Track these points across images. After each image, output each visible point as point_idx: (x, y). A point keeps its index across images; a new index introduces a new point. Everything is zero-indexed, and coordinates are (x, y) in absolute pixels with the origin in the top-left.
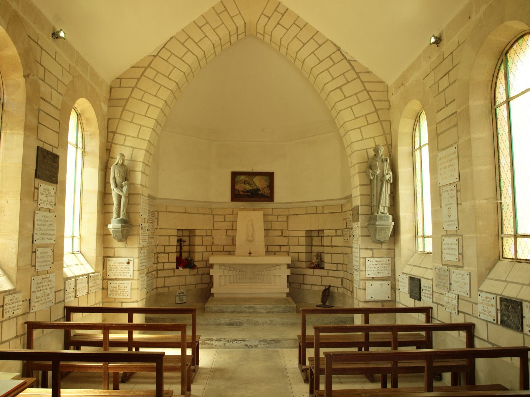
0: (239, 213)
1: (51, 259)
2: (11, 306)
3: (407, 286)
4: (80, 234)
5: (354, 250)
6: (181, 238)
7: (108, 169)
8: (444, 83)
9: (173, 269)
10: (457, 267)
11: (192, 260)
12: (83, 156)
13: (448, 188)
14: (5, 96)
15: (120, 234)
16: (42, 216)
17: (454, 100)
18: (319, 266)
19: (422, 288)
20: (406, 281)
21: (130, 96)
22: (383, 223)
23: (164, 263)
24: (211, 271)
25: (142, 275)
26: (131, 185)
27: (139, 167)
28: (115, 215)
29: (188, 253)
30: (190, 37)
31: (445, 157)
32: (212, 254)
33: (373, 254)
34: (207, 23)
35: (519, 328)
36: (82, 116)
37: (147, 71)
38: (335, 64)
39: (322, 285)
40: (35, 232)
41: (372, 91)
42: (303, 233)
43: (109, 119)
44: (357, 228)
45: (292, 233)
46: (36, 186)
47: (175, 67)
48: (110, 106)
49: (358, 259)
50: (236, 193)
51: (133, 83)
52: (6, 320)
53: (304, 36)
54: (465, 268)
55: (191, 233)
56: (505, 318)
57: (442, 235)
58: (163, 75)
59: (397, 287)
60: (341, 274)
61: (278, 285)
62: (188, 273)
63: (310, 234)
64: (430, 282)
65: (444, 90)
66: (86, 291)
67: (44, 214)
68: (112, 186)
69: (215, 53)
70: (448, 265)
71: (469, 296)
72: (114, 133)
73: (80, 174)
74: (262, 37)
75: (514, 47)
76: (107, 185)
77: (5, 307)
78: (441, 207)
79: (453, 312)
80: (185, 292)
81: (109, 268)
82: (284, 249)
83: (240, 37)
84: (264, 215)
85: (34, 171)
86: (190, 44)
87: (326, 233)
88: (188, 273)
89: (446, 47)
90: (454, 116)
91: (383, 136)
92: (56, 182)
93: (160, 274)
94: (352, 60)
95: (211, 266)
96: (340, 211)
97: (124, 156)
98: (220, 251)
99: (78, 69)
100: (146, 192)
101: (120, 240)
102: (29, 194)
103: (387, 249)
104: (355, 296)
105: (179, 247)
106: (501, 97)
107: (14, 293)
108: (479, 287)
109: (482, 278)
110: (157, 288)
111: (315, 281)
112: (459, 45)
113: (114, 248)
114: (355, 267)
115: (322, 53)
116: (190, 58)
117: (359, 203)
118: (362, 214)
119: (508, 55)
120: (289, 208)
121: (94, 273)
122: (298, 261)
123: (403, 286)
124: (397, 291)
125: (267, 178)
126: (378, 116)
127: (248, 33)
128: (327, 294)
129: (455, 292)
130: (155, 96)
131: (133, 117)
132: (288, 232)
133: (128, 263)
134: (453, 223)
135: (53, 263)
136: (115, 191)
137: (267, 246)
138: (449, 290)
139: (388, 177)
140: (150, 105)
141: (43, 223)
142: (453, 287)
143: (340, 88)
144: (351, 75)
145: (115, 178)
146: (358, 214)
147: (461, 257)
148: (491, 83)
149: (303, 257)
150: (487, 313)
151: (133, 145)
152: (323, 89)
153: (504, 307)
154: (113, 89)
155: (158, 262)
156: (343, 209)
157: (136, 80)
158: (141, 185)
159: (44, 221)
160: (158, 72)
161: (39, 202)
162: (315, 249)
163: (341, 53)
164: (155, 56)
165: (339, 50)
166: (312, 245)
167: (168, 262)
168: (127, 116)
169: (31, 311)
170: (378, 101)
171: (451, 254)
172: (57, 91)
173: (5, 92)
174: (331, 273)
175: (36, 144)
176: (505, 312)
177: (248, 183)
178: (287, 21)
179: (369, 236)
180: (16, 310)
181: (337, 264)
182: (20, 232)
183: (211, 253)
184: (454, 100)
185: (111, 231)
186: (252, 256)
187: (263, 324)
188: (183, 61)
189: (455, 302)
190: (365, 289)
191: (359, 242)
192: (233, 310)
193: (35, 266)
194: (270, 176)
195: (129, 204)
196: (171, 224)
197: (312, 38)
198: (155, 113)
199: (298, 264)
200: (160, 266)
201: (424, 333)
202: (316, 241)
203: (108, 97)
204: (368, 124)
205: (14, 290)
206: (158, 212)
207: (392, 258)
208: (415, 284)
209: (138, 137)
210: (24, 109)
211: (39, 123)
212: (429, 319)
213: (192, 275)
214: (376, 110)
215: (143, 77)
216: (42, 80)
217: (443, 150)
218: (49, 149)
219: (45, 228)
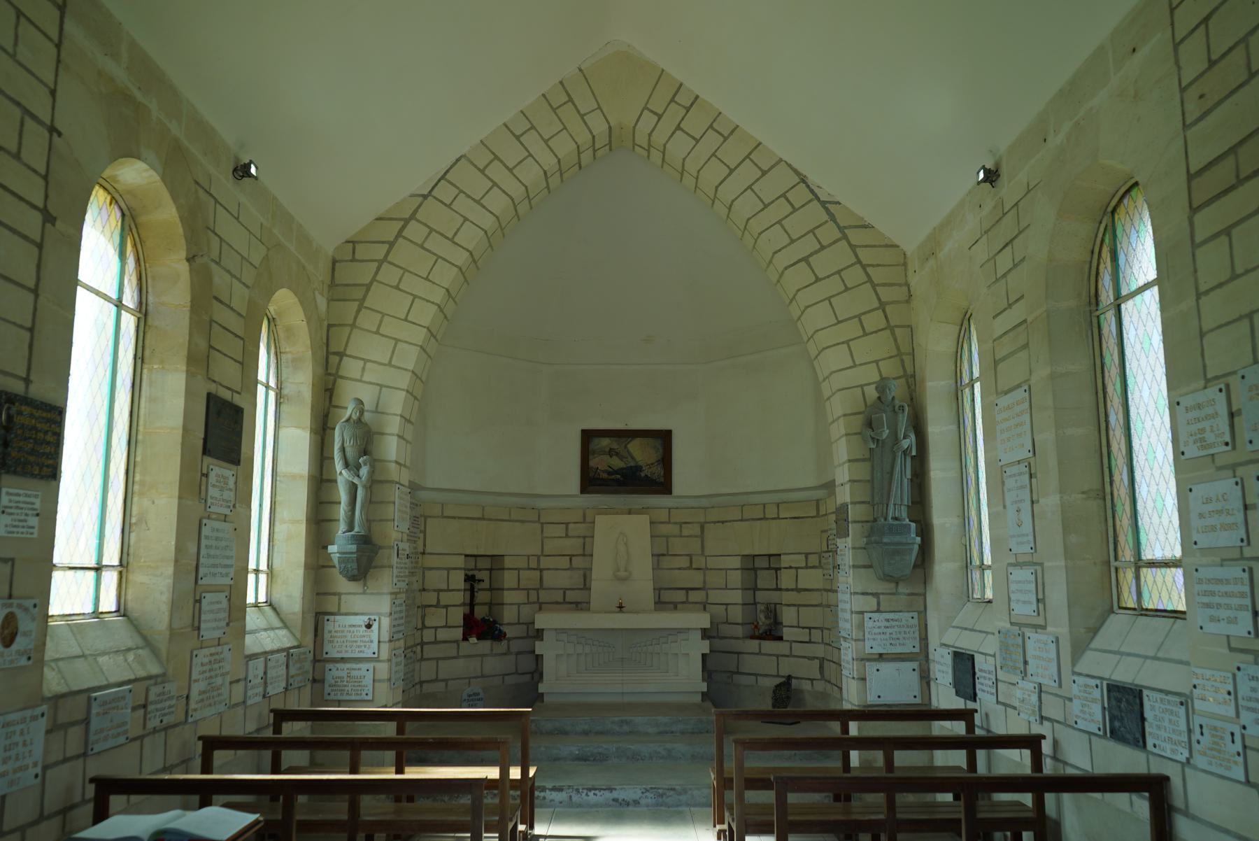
0: (599, 519)
1: (224, 615)
2: (159, 706)
3: (950, 671)
4: (270, 566)
5: (840, 595)
6: (470, 573)
7: (328, 431)
8: (1004, 262)
9: (456, 642)
10: (1036, 627)
11: (495, 622)
12: (278, 404)
13: (1015, 469)
14: (151, 299)
15: (355, 565)
16: (213, 530)
17: (1022, 297)
18: (772, 633)
19: (978, 674)
20: (949, 660)
21: (374, 279)
22: (897, 539)
23: (436, 628)
24: (537, 643)
25: (398, 652)
26: (375, 464)
27: (393, 425)
28: (342, 527)
29: (486, 608)
30: (496, 157)
31: (1008, 408)
32: (540, 609)
33: (879, 604)
34: (533, 127)
35: (1139, 741)
36: (278, 322)
37: (409, 226)
38: (795, 210)
39: (778, 676)
40: (202, 560)
41: (873, 266)
42: (736, 562)
43: (329, 326)
44: (847, 549)
45: (712, 563)
46: (205, 471)
47: (466, 219)
48: (331, 300)
49: (848, 616)
50: (592, 474)
51: (380, 251)
52: (149, 734)
53: (732, 153)
54: (1049, 629)
55: (496, 563)
56: (1117, 724)
57: (1010, 565)
58: (442, 235)
59: (932, 676)
60: (819, 651)
61: (683, 673)
62: (487, 651)
63: (751, 565)
64: (991, 660)
65: (1004, 275)
66: (284, 684)
67: (217, 525)
68: (339, 466)
69: (548, 187)
70: (1020, 625)
71: (1056, 685)
72: (341, 355)
73: (277, 443)
74: (645, 153)
75: (1125, 201)
76: (326, 462)
77: (150, 708)
78: (1005, 507)
79: (1032, 719)
80: (480, 691)
81: (327, 636)
82: (695, 596)
83: (599, 153)
84: (651, 523)
85: (201, 442)
86: (496, 172)
87: (785, 561)
88: (487, 651)
89: (1009, 188)
90: (1024, 326)
91: (888, 332)
92: (236, 462)
93: (430, 651)
94: (830, 202)
95: (539, 634)
96: (814, 514)
97: (362, 403)
98: (557, 603)
99: (276, 231)
100: (405, 477)
101: (353, 578)
102: (193, 487)
103: (909, 595)
104: (845, 696)
105: (468, 593)
106: (1107, 296)
107: (163, 682)
108: (1074, 665)
109: (1078, 650)
110: (421, 683)
111: (763, 665)
112: (1029, 191)
113: (339, 594)
114: (843, 634)
115: (770, 188)
116: (497, 202)
117: (848, 500)
118: (855, 522)
119: (1116, 217)
120: (705, 508)
121: (298, 647)
122: (727, 622)
123: (943, 672)
124: (932, 684)
125: (658, 443)
126: (886, 317)
127: (616, 141)
128: (785, 691)
129: (1034, 679)
130: (427, 279)
131: (381, 322)
132: (703, 559)
133: (369, 626)
134: (1025, 539)
135: (228, 624)
136: (343, 476)
137: (658, 590)
138: (1024, 673)
139: (905, 444)
140: (415, 297)
141: (214, 543)
142: (1030, 669)
143: (805, 259)
144: (829, 233)
145: (343, 450)
146: (846, 520)
147: (1041, 606)
148: (1087, 266)
149: (737, 614)
150: (1087, 716)
151: (380, 378)
152: (770, 262)
153: (1114, 703)
154: (337, 265)
155: (424, 627)
156: (816, 508)
157: (387, 246)
158: (397, 462)
159: (217, 539)
160: (432, 230)
161: (209, 501)
162: (762, 597)
163: (808, 186)
164: (425, 197)
165: (803, 180)
166: (755, 589)
167: (446, 626)
168: (367, 320)
169: (190, 720)
170: (884, 285)
171: (1024, 602)
172: (240, 281)
173: (150, 290)
174: (798, 649)
175: (204, 388)
176: (1116, 713)
177: (617, 454)
178: (696, 123)
179: (870, 567)
180: (165, 715)
181: (810, 628)
182: (176, 561)
183: (537, 606)
184: (1022, 297)
185: (335, 559)
186: (625, 610)
187: (651, 758)
188: (484, 207)
189: (1034, 698)
190: (864, 679)
191: (850, 580)
192: (586, 727)
193: (199, 628)
194: (665, 437)
195: (370, 502)
196: (451, 544)
197: (748, 157)
198: (426, 315)
199: (725, 630)
200: (428, 635)
201: (1027, 799)
202: (765, 579)
203: (328, 281)
204: (865, 334)
205: (164, 675)
206: (426, 518)
207: (919, 612)
208: (964, 664)
209: (390, 364)
210: (186, 322)
211: (211, 347)
212: (971, 727)
213: (496, 655)
214: (882, 306)
215: (400, 240)
216: (217, 263)
217: (1006, 393)
218: (226, 395)
219: (218, 552)
